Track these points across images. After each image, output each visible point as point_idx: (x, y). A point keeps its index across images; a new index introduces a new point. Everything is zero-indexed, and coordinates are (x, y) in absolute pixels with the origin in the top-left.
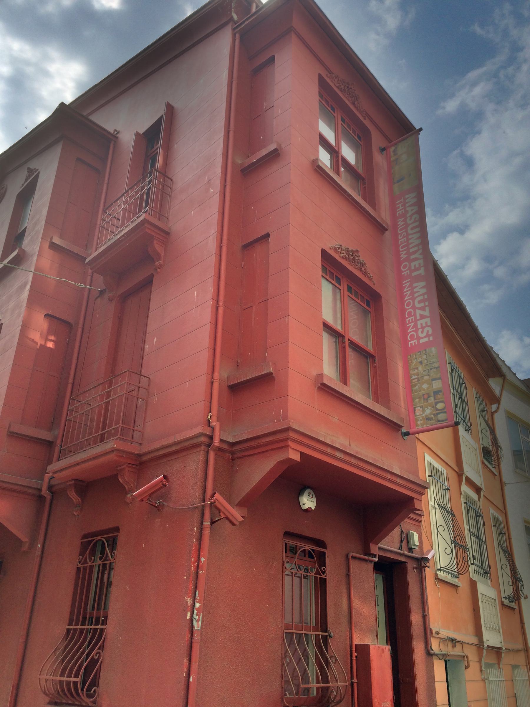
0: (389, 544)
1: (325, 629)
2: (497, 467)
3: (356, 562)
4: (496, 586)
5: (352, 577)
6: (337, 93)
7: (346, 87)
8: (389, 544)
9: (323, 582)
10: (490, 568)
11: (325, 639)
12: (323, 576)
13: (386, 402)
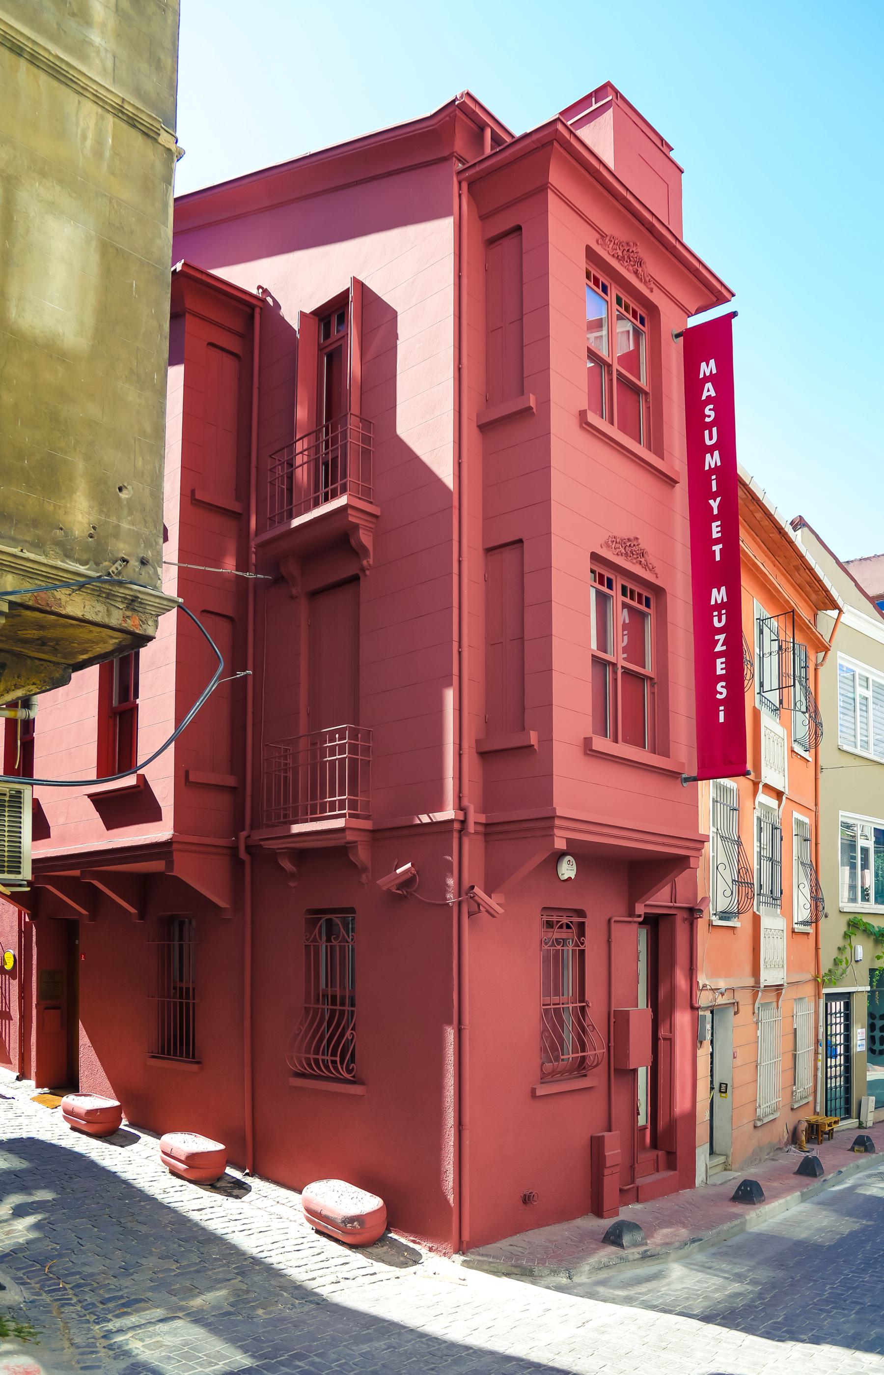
0: (659, 899)
1: (582, 999)
2: (813, 751)
3: (620, 925)
4: (787, 725)
5: (613, 944)
6: (452, 926)
7: (625, 252)
8: (659, 899)
9: (582, 952)
10: (781, 893)
11: (583, 1009)
12: (582, 947)
13: (666, 753)
